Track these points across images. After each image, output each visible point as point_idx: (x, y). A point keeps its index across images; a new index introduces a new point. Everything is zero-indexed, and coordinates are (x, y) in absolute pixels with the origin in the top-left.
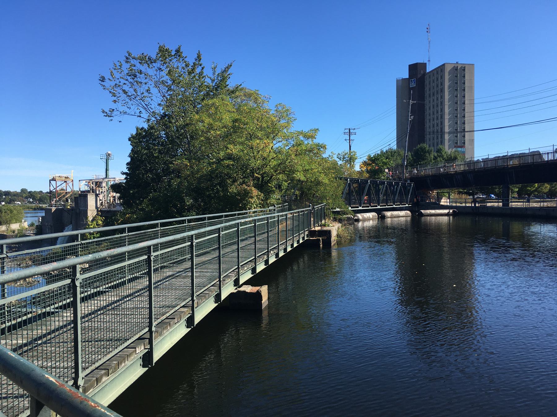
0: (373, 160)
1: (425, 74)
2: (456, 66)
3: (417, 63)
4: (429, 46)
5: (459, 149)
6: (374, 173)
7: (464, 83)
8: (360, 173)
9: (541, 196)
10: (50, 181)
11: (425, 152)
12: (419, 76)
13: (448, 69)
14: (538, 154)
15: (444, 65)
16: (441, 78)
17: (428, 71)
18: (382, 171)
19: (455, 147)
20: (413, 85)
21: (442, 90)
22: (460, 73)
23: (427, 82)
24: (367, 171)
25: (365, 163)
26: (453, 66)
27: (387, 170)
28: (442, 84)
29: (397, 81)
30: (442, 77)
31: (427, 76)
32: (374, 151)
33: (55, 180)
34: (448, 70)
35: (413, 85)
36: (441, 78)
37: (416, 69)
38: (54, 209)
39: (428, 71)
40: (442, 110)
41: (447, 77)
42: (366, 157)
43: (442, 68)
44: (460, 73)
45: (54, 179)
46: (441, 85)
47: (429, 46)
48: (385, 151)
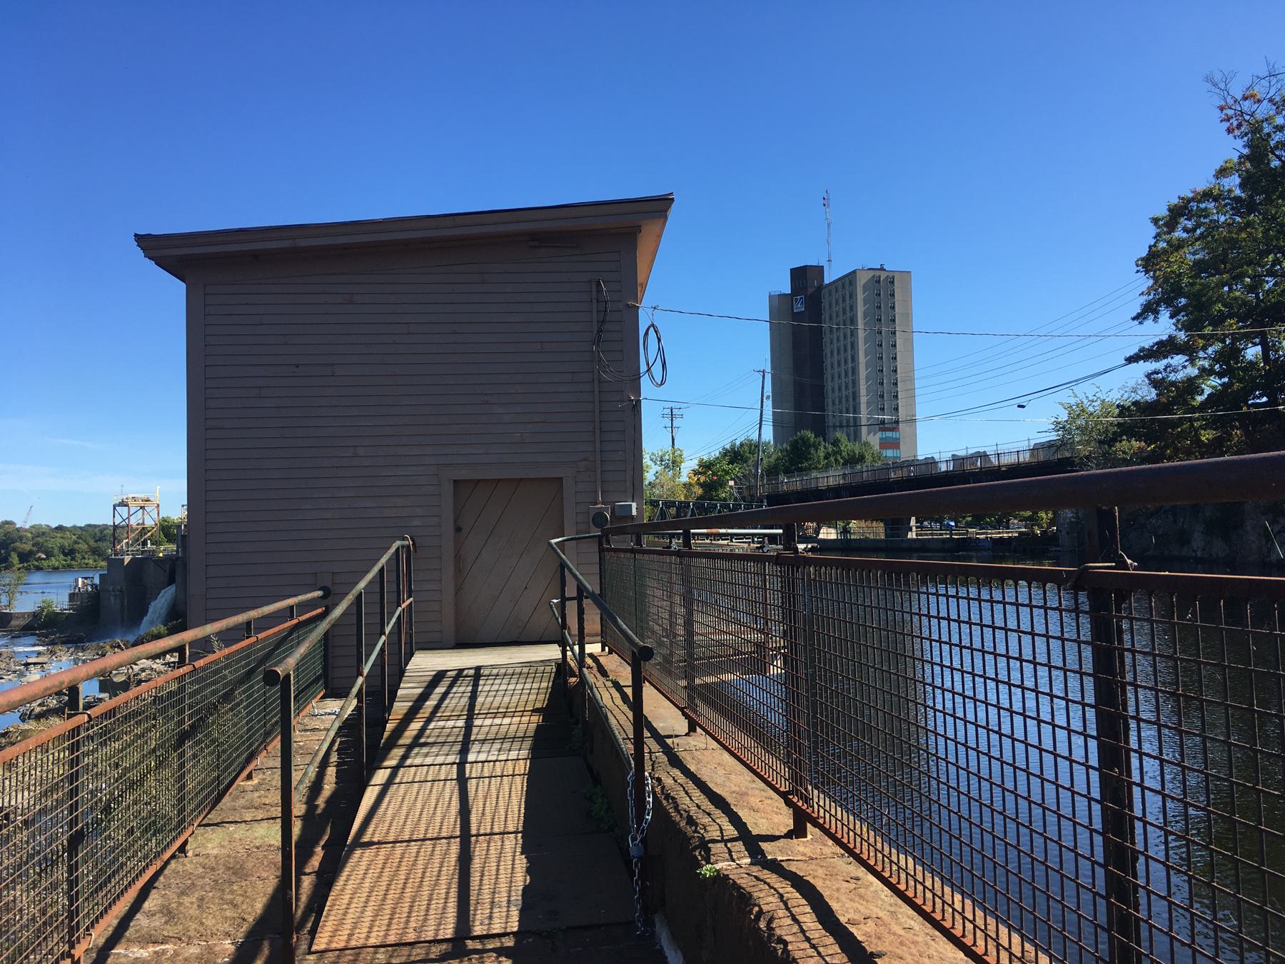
0: (706, 466)
1: (821, 287)
2: (877, 273)
3: (806, 267)
4: (829, 235)
5: (889, 434)
6: (710, 488)
7: (893, 308)
8: (687, 486)
9: (25, 645)
10: (114, 507)
11: (809, 446)
12: (810, 290)
13: (862, 280)
14: (984, 456)
15: (854, 272)
16: (851, 296)
17: (827, 281)
18: (722, 484)
19: (881, 430)
20: (799, 307)
21: (853, 321)
22: (884, 290)
23: (825, 303)
24: (702, 485)
25: (696, 473)
26: (871, 273)
27: (732, 483)
28: (853, 308)
29: (771, 297)
30: (852, 296)
31: (825, 292)
32: (712, 451)
33: (127, 505)
34: (863, 282)
35: (799, 307)
36: (851, 296)
37: (804, 277)
38: (127, 559)
39: (827, 281)
40: (854, 358)
41: (860, 297)
42: (696, 462)
43: (851, 278)
44: (884, 290)
45: (123, 504)
46: (851, 309)
47: (829, 235)
48: (738, 443)
